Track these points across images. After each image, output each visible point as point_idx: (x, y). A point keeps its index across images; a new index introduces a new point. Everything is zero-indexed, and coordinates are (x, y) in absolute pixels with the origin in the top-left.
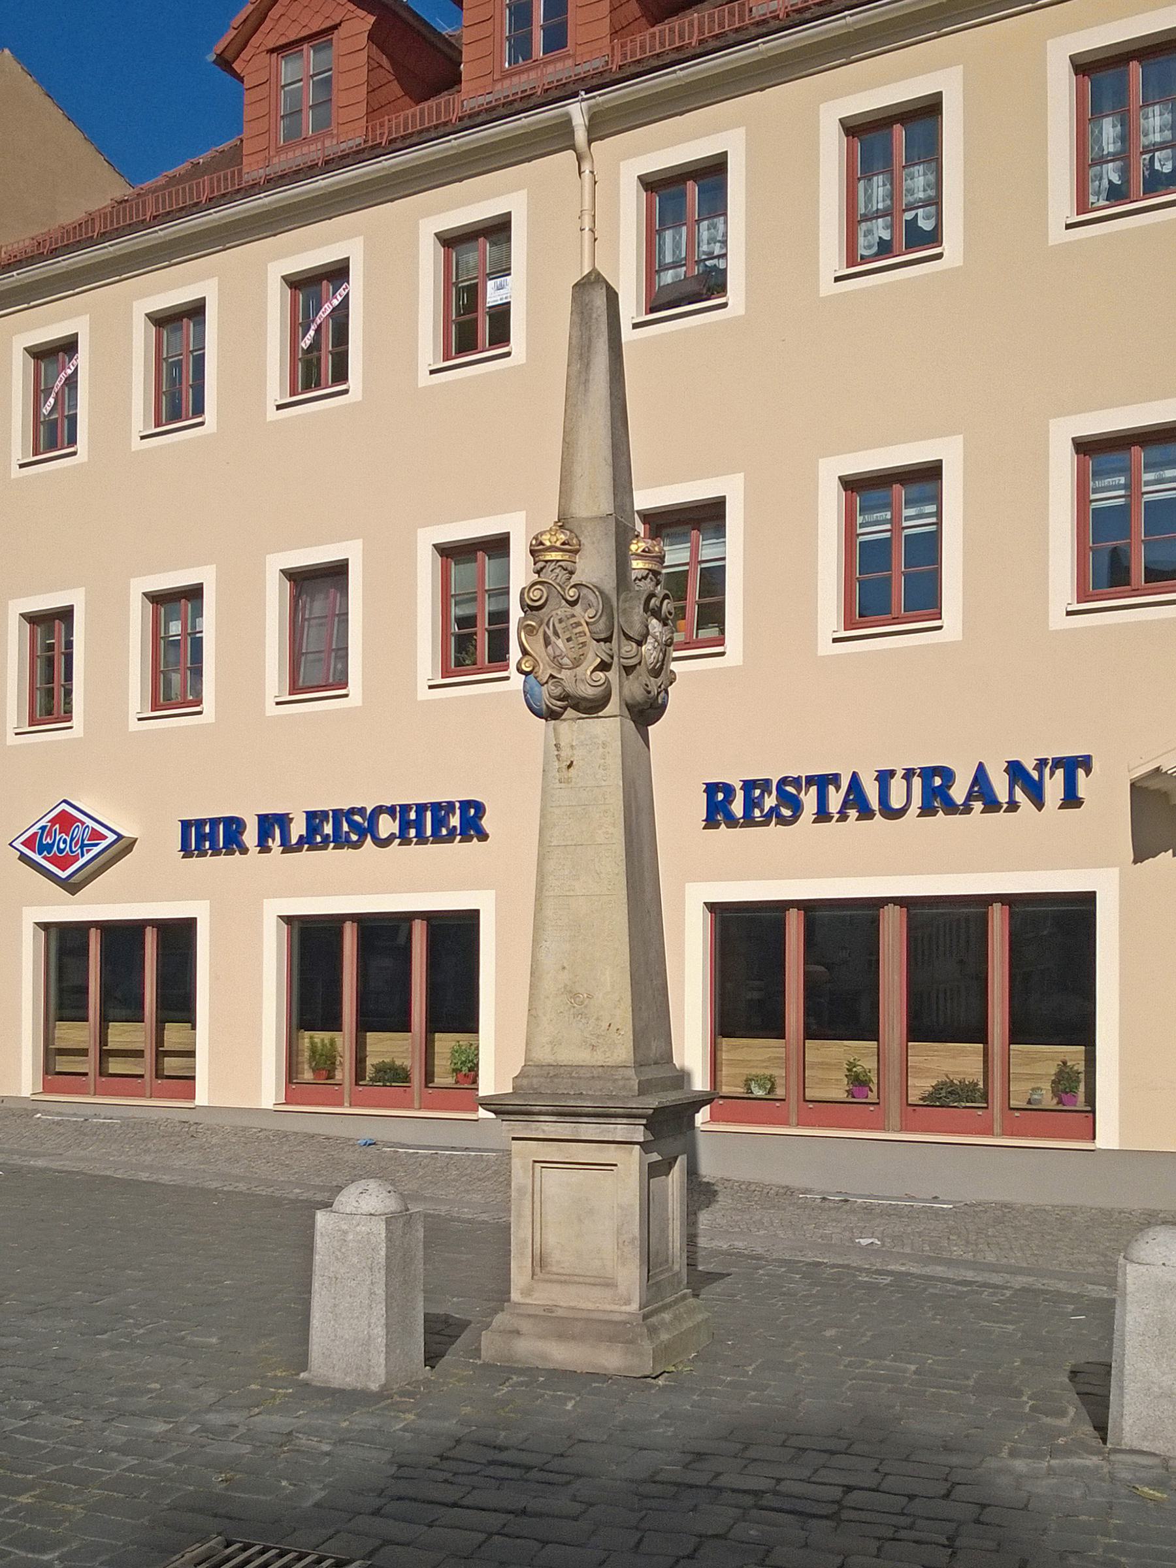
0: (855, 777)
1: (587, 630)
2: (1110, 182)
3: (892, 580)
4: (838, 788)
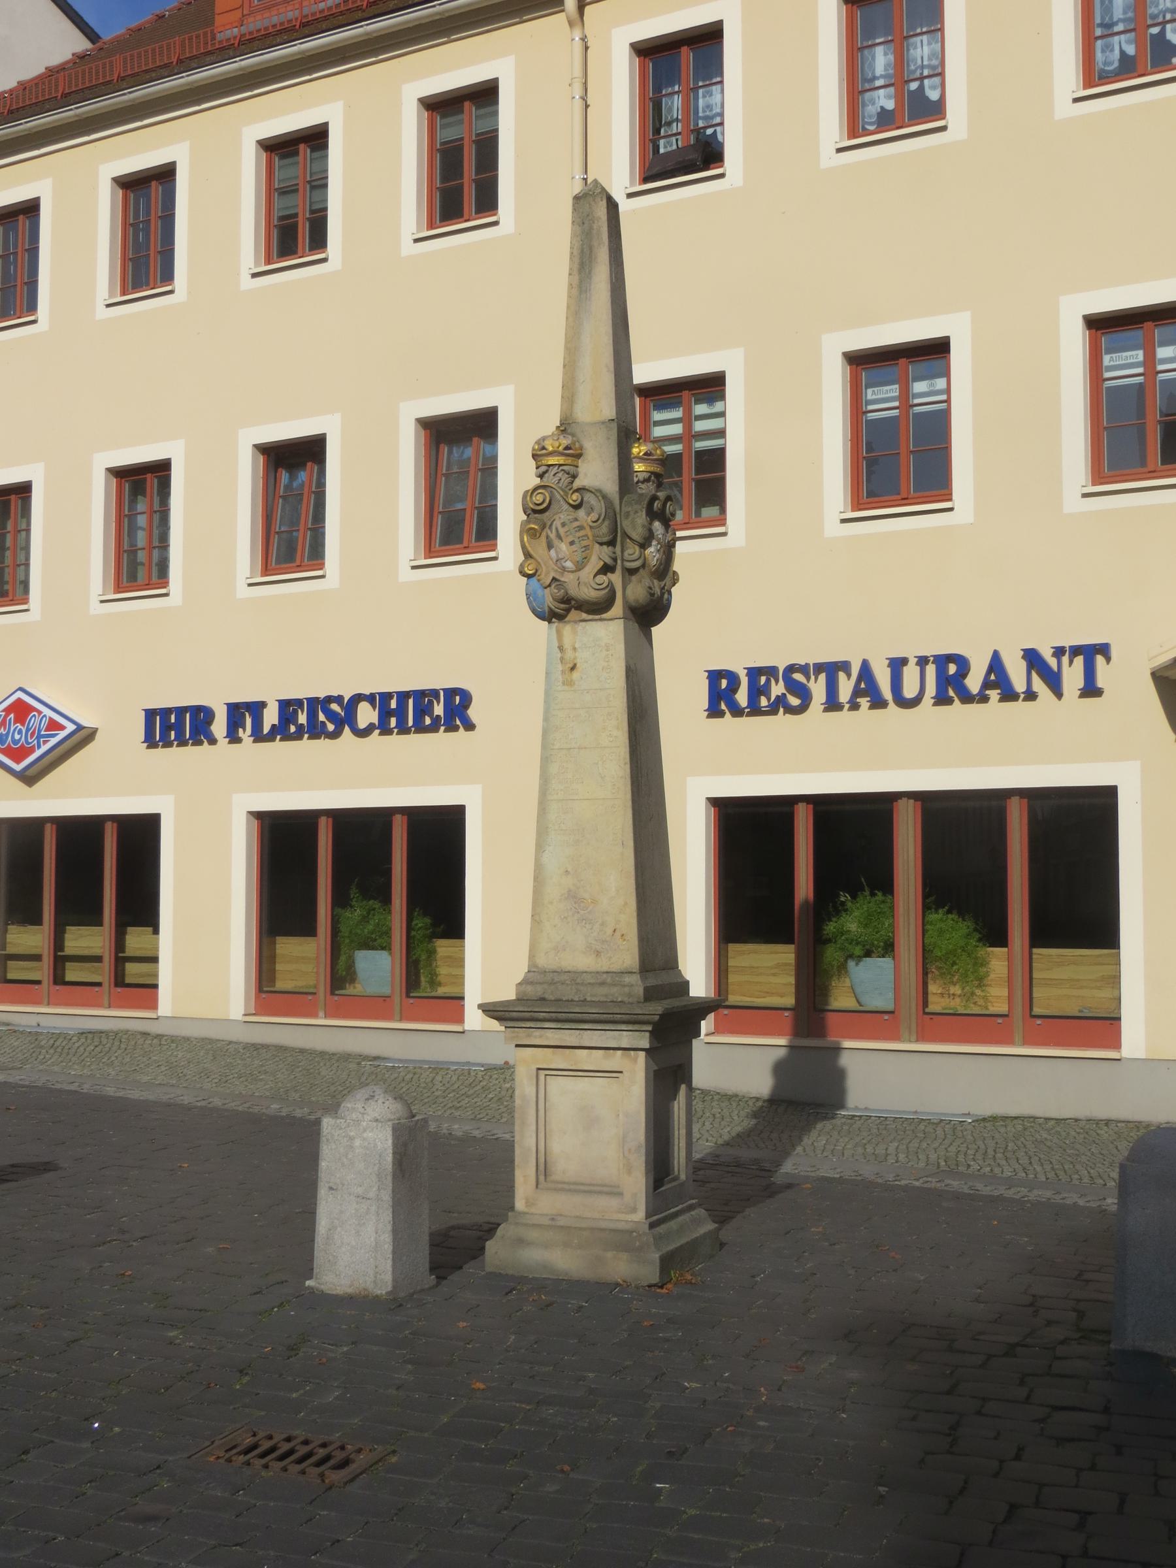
0: (865, 668)
1: (590, 534)
2: (1122, 52)
3: (899, 460)
4: (849, 676)
